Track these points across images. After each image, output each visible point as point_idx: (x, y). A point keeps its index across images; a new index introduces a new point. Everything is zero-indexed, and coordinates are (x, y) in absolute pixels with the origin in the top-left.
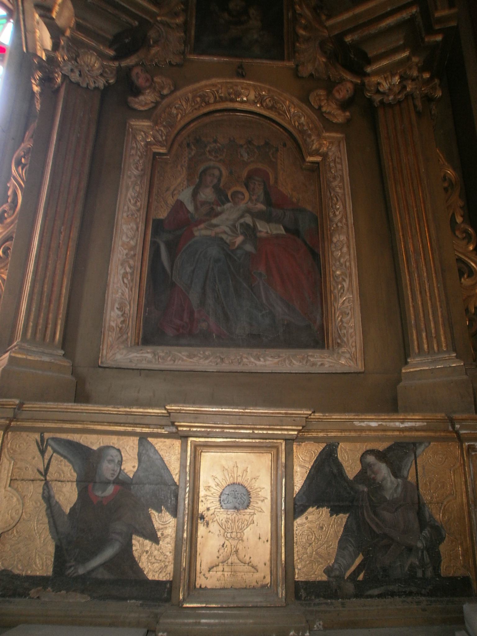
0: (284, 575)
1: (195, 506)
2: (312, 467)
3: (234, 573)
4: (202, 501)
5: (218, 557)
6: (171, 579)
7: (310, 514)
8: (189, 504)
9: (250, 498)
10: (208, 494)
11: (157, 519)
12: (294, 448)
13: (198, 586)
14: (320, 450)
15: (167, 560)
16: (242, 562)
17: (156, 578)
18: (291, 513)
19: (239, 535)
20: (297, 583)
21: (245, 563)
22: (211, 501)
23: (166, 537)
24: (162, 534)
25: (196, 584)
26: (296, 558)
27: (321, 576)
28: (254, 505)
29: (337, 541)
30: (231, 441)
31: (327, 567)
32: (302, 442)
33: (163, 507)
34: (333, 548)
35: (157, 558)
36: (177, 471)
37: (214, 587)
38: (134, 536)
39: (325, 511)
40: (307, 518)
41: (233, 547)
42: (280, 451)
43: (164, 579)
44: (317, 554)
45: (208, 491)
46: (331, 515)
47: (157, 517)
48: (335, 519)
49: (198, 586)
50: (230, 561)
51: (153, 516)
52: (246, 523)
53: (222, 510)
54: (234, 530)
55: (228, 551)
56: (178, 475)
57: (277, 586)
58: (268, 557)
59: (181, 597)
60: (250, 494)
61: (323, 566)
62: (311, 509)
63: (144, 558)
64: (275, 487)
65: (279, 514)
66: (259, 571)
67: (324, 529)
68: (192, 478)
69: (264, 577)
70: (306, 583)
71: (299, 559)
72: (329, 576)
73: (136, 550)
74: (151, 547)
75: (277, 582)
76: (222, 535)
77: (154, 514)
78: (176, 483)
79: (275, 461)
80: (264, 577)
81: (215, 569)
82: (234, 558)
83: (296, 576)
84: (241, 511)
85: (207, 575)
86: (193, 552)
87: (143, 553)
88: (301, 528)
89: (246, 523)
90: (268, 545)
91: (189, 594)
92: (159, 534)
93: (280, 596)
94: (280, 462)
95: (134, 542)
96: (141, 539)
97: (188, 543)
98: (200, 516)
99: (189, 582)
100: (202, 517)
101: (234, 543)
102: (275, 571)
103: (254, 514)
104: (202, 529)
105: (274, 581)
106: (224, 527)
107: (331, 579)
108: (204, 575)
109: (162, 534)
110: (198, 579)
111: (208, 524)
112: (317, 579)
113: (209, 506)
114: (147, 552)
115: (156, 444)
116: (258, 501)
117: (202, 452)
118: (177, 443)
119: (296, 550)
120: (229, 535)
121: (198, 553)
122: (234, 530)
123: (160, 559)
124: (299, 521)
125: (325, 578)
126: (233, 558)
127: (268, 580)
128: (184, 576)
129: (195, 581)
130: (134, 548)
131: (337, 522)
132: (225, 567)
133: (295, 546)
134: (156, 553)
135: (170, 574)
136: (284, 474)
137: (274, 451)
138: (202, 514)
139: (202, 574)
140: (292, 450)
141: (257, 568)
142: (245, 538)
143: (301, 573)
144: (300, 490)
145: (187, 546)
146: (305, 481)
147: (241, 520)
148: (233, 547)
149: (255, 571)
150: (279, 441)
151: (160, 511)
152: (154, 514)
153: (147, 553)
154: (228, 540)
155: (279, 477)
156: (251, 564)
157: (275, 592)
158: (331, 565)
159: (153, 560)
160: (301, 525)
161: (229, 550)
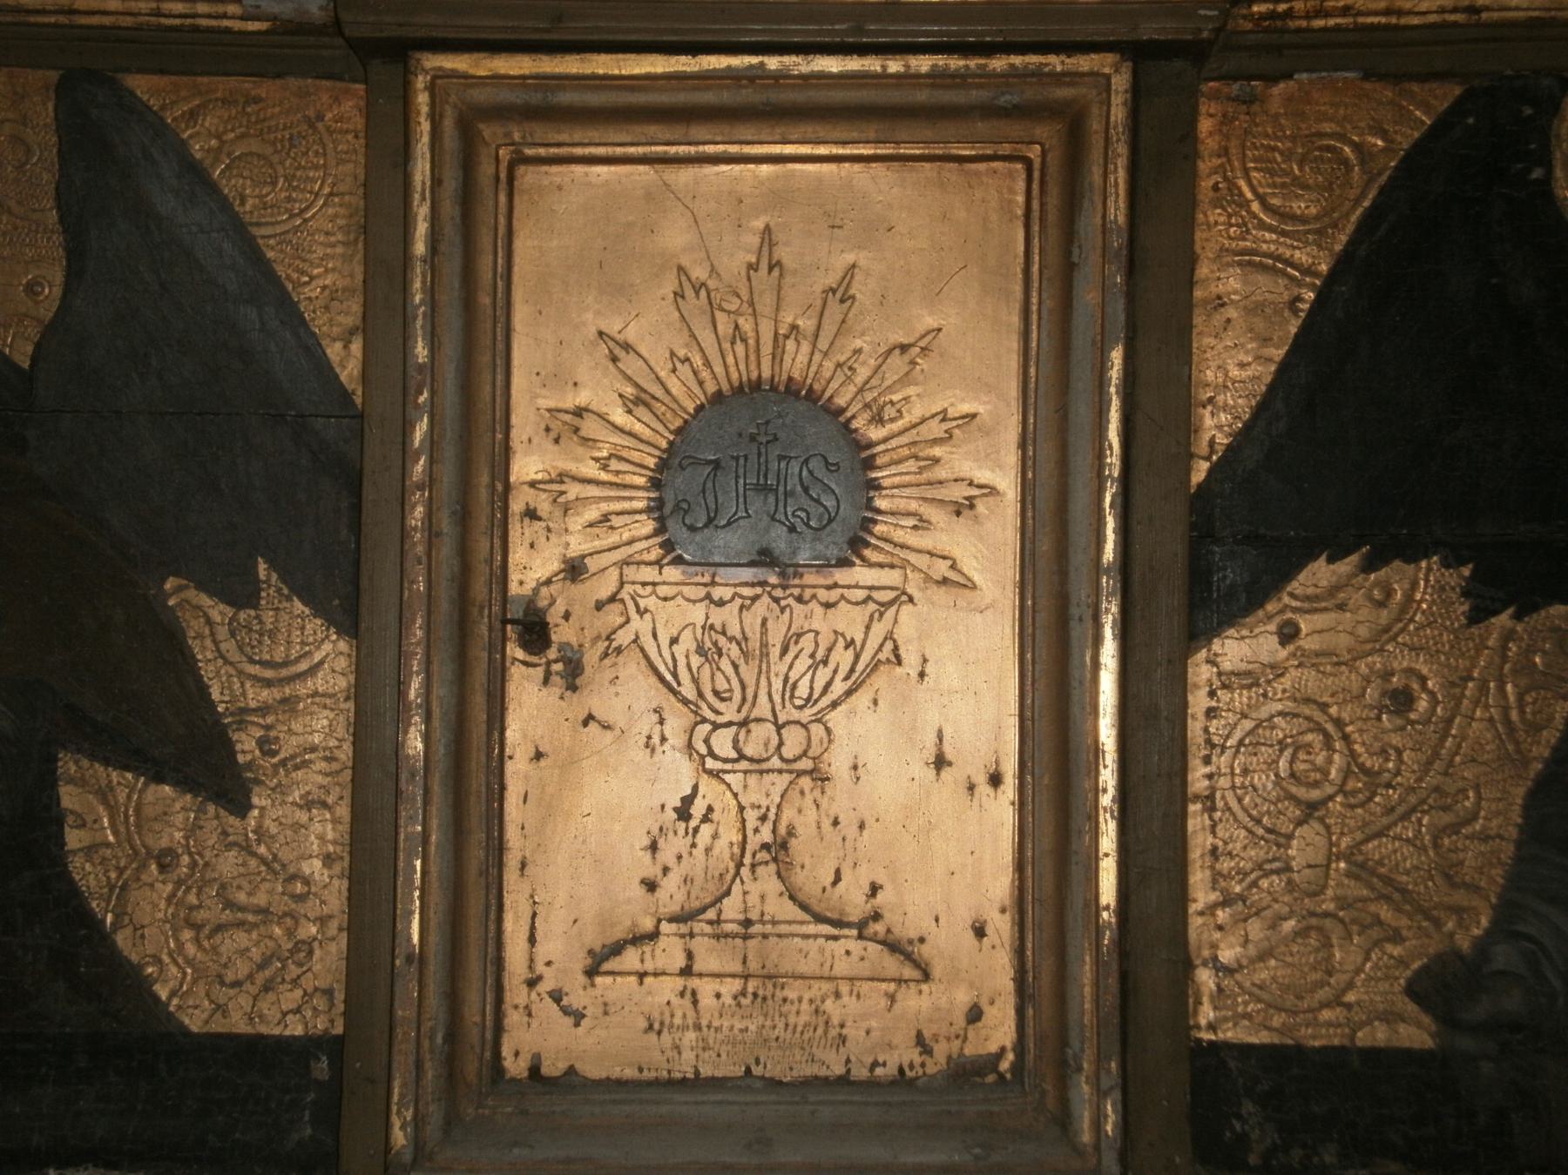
0: (1111, 999)
1: (482, 546)
4: (531, 514)
5: (651, 886)
6: (339, 1029)
7: (1312, 604)
9: (874, 485)
10: (571, 467)
11: (229, 646)
12: (1205, 125)
13: (515, 1067)
14: (1406, 138)
15: (312, 908)
16: (819, 919)
17: (237, 1023)
18: (1170, 600)
19: (794, 741)
20: (1212, 1061)
21: (838, 923)
22: (592, 514)
23: (297, 763)
24: (266, 745)
25: (506, 1051)
26: (1201, 894)
27: (1390, 1017)
28: (899, 535)
29: (1519, 793)
31: (1439, 958)
32: (1272, 79)
33: (262, 567)
34: (1484, 837)
35: (242, 897)
37: (630, 1073)
38: (68, 764)
39: (1427, 583)
40: (1288, 634)
41: (751, 817)
42: (1097, 143)
43: (296, 1029)
45: (570, 443)
46: (1478, 615)
47: (223, 632)
48: (1508, 636)
50: (731, 908)
51: (193, 627)
52: (842, 658)
53: (673, 573)
54: (763, 708)
55: (721, 846)
56: (356, 347)
57: (1064, 1070)
58: (1001, 885)
59: (399, 1138)
60: (869, 464)
61: (1414, 950)
62: (1319, 573)
63: (153, 899)
64: (484, 215)
65: (1080, 592)
66: (937, 972)
67: (1423, 704)
70: (1280, 1060)
71: (1226, 903)
72: (1448, 1020)
73: (89, 851)
74: (192, 830)
75: (1064, 1042)
76: (676, 739)
77: (202, 616)
78: (346, 396)
79: (1053, 216)
81: (630, 959)
82: (761, 891)
83: (1207, 1014)
84: (810, 578)
85: (576, 999)
86: (476, 855)
87: (144, 866)
88: (1240, 699)
89: (842, 658)
90: (1002, 809)
91: (451, 1120)
92: (246, 745)
93: (1086, 1137)
94: (1089, 224)
95: (69, 797)
96: (121, 781)
97: (436, 788)
98: (515, 612)
99: (454, 1033)
101: (763, 791)
102: (1046, 979)
103: (903, 597)
106: (688, 691)
107: (1466, 1043)
108: (557, 996)
109: (266, 745)
110: (513, 1018)
112: (1363, 1038)
113: (578, 545)
114: (166, 860)
116: (928, 511)
117: (520, 160)
118: (345, 107)
120: (723, 743)
122: (763, 708)
123: (261, 899)
124: (1234, 649)
125: (1415, 1033)
126: (754, 889)
127: (999, 1031)
128: (416, 1004)
129: (499, 1029)
130: (74, 838)
132: (700, 945)
134: (229, 864)
136: (1119, 307)
137: (1041, 143)
138: (530, 603)
139: (544, 987)
140: (1189, 135)
141: (926, 951)
142: (838, 763)
144: (1243, 438)
145: (440, 815)
146: (1284, 368)
147: (807, 642)
148: (751, 817)
149: (909, 972)
150: (1084, 63)
151: (243, 595)
152: (202, 616)
153: (163, 868)
154: (715, 775)
156: (878, 928)
157: (1051, 1103)
159: (212, 912)
160: (1248, 678)
161: (731, 835)
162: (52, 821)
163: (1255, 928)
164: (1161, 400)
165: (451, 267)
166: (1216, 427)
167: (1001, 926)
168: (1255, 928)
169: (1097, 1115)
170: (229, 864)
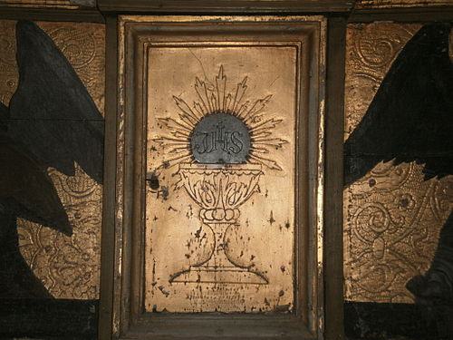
0: (321, 289)
2: (388, 76)
3: (220, 285)
4: (154, 149)
5: (188, 256)
7: (379, 175)
8: (125, 155)
9: (253, 140)
12: (348, 36)
13: (149, 309)
14: (407, 40)
15: (90, 263)
18: (338, 173)
19: (229, 214)
26: (347, 259)
30: (211, 21)
31: (416, 277)
34: (429, 242)
36: (102, 90)
38: (20, 221)
39: (412, 169)
40: (372, 184)
41: (217, 236)
44: (393, 252)
47: (64, 183)
48: (436, 184)
49: (149, 309)
50: (211, 262)
51: (56, 181)
52: (243, 190)
53: (194, 166)
54: (220, 205)
56: (103, 100)
57: (307, 309)
58: (289, 256)
60: (251, 134)
61: (408, 275)
62: (381, 166)
63: (44, 260)
65: (312, 172)
66: (270, 281)
67: (411, 204)
68: (130, 101)
69: (282, 294)
72: (418, 296)
75: (308, 302)
76: (195, 214)
77: (59, 178)
78: (100, 114)
80: (282, 294)
81: (182, 277)
83: (349, 293)
86: (137, 247)
88: (359, 202)
89: (243, 190)
90: (289, 235)
92: (71, 215)
94: (315, 64)
95: (20, 231)
99: (131, 300)
100: (154, 183)
104: (153, 204)
105: (300, 301)
107: (424, 302)
108: (161, 288)
111: (165, 195)
113: (166, 159)
114: (48, 249)
115: (56, 33)
118: (100, 31)
119: (347, 244)
121: (148, 249)
122: (220, 205)
123: (75, 260)
125: (409, 299)
127: (289, 298)
128: (120, 290)
129: (144, 298)
130: (21, 243)
131: (440, 193)
133: (346, 237)
134: (66, 250)
135: (95, 287)
136: (323, 89)
137: (301, 41)
138: (154, 174)
142: (242, 221)
143: (359, 283)
144: (359, 126)
145: (126, 235)
149: (263, 281)
150: (313, 18)
151: (69, 171)
155: (312, 98)
158: (423, 273)
160: (361, 196)
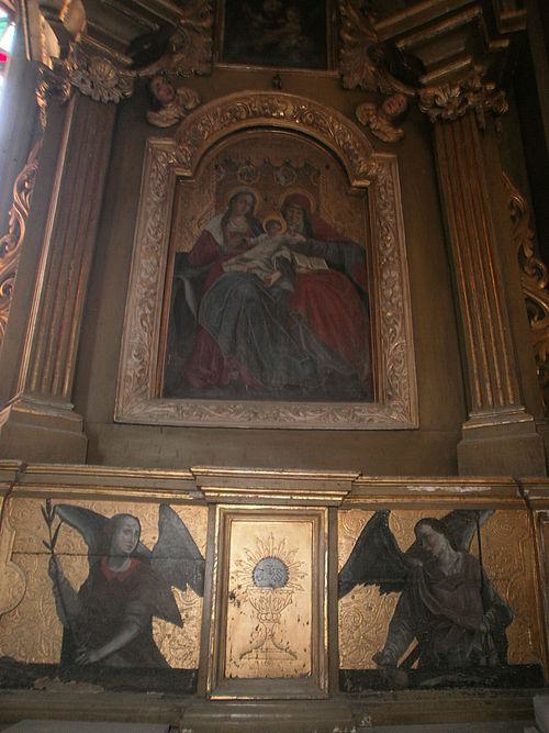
7: (356, 592)
23: (191, 619)
24: (187, 616)
38: (154, 618)
39: (374, 589)
40: (353, 597)
50: (264, 647)
58: (309, 642)
61: (373, 652)
62: (357, 587)
63: (166, 643)
70: (353, 671)
77: (177, 592)
82: (269, 644)
92: (183, 616)
95: (154, 624)
101: (270, 625)
107: (381, 668)
109: (187, 616)
114: (169, 636)
118: (204, 511)
124: (344, 600)
128: (212, 664)
134: (179, 637)
142: (282, 620)
145: (216, 630)
160: (347, 605)
162: (151, 628)
163: (349, 649)
164: (333, 547)
165: (221, 538)
166: (341, 564)
167: (309, 649)
168: (349, 649)
169: (324, 683)
170: (179, 637)
